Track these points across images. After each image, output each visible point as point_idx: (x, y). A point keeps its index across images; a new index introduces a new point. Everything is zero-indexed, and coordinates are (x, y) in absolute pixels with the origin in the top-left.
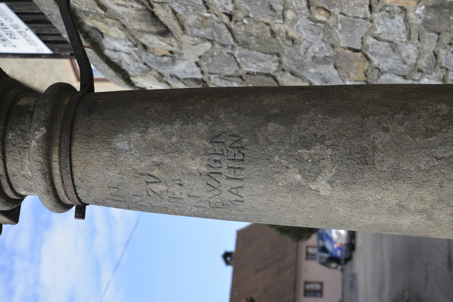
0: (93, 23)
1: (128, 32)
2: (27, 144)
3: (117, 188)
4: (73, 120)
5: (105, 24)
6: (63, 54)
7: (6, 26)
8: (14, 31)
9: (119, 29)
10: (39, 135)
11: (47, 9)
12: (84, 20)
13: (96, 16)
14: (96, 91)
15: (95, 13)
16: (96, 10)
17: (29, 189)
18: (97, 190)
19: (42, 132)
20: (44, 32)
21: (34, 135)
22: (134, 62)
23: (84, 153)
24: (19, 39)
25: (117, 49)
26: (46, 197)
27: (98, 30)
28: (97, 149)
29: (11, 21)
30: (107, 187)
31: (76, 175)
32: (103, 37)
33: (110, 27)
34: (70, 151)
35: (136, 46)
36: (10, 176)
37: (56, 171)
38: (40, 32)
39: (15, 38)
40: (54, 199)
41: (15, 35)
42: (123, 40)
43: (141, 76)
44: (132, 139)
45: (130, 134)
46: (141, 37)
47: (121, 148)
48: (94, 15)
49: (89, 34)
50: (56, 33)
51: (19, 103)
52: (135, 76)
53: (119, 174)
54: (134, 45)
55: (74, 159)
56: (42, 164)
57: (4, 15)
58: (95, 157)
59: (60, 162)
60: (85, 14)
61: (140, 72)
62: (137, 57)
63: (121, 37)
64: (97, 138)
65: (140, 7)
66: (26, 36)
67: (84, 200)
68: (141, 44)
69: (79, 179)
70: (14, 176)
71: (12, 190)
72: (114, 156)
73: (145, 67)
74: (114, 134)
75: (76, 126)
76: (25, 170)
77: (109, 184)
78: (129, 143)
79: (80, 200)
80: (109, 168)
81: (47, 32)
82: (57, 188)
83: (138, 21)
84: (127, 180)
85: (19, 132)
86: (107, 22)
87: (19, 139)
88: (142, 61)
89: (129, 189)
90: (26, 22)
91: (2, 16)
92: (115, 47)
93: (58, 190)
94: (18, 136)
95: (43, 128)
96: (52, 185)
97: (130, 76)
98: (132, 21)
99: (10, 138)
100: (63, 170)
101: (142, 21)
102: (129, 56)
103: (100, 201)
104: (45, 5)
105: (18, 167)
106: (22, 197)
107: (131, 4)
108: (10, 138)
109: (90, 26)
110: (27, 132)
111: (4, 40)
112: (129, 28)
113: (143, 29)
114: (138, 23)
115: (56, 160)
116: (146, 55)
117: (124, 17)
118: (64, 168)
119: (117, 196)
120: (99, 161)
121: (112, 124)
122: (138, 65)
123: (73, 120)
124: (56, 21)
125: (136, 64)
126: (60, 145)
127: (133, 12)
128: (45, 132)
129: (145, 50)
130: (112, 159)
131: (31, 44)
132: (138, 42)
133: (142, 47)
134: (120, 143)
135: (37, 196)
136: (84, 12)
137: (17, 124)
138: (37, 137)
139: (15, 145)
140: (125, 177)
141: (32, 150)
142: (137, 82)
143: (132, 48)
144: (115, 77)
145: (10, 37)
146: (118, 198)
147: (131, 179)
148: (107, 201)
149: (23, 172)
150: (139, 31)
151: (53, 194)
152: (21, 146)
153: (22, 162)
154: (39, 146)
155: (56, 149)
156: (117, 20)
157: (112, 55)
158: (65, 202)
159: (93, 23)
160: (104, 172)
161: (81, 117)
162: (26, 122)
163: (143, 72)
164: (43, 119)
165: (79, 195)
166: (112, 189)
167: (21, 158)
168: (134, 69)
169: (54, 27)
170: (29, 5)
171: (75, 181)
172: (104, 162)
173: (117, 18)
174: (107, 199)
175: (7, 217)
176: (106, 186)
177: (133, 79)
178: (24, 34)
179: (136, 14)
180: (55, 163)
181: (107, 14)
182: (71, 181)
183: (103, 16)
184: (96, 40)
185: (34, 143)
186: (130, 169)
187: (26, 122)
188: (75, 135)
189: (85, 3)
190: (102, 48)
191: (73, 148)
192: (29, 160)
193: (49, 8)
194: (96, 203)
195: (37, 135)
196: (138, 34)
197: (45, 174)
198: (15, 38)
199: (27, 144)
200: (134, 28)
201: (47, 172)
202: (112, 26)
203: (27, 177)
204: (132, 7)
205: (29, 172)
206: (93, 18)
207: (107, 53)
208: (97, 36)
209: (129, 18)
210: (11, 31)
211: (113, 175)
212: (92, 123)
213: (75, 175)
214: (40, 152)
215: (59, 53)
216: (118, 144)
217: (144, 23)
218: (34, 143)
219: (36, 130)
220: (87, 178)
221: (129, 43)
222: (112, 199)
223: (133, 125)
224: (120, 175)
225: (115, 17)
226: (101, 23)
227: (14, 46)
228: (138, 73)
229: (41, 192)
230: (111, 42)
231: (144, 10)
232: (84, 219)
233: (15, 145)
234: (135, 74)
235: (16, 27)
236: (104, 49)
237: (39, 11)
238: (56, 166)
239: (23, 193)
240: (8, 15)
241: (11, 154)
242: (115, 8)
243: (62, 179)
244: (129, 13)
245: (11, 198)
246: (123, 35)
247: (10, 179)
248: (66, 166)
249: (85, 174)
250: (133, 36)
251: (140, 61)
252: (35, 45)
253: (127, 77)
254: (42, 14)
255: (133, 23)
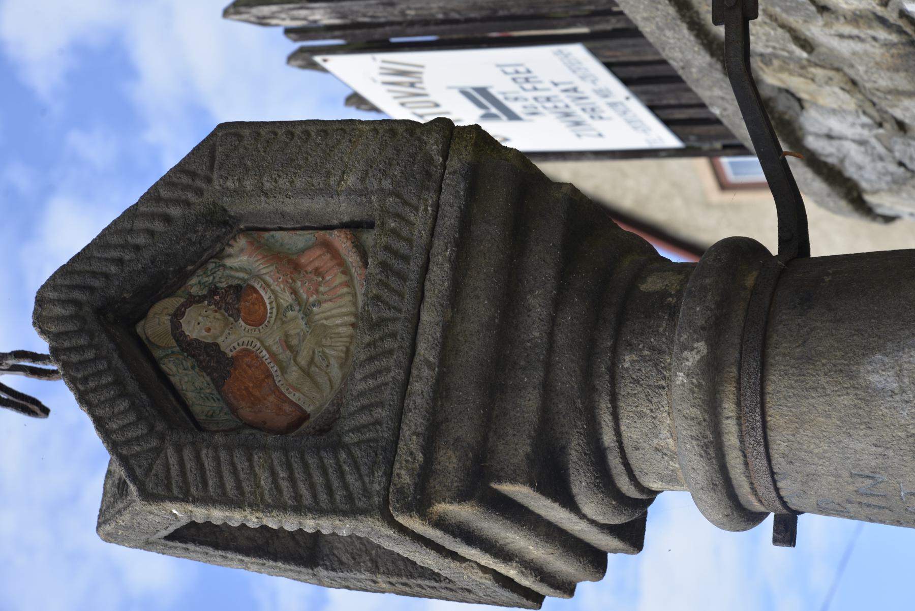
0: (781, 80)
1: (864, 95)
2: (664, 378)
3: (873, 478)
4: (767, 322)
5: (809, 81)
6: (706, 146)
7: (582, 92)
8: (601, 103)
9: (843, 89)
10: (692, 359)
11: (678, 55)
12: (761, 73)
13: (788, 64)
14: (813, 254)
15: (786, 57)
16: (788, 52)
17: (669, 479)
18: (824, 483)
19: (699, 352)
20: (665, 102)
21: (680, 359)
22: (873, 161)
23: (794, 399)
24: (610, 119)
25: (833, 134)
26: (709, 498)
27: (793, 95)
28: (824, 388)
29: (594, 82)
30: (848, 475)
31: (775, 447)
32: (802, 108)
33: (820, 86)
34: (763, 394)
35: (880, 125)
36: (628, 450)
37: (731, 439)
38: (657, 103)
39: (601, 118)
40: (725, 501)
41: (603, 112)
42: (850, 112)
43: (890, 190)
44: (906, 366)
45: (901, 354)
46: (893, 106)
47: (880, 386)
48: (784, 62)
49: (771, 104)
50: (694, 102)
51: (643, 287)
52: (875, 192)
53: (875, 445)
54: (876, 123)
55: (770, 412)
56: (699, 424)
57: (579, 69)
58: (820, 408)
59: (739, 418)
60: (762, 61)
61: (888, 183)
62: (881, 149)
63: (845, 107)
64: (824, 365)
65: (894, 38)
66: (625, 113)
67: (794, 503)
68: (893, 122)
69: (784, 456)
70: (637, 449)
71: (631, 480)
72: (863, 405)
73: (902, 170)
74: (863, 355)
75: (775, 337)
76: (662, 436)
77: (854, 467)
78: (899, 375)
79: (784, 504)
80: (852, 432)
81: (673, 102)
82: (732, 476)
83: (888, 69)
84: (896, 460)
85: (646, 352)
86: (814, 75)
87: (647, 369)
88: (894, 158)
89: (901, 480)
90: (627, 82)
91: (574, 72)
92: (830, 129)
93: (734, 482)
94: (645, 361)
95: (700, 344)
96: (723, 470)
97: (865, 191)
98: (874, 70)
99: (627, 365)
100: (747, 438)
101: (897, 70)
102: (862, 149)
103: (831, 506)
104: (673, 48)
105: (646, 430)
106: (652, 494)
107: (871, 32)
108: (627, 365)
109: (773, 87)
110: (664, 352)
111: (577, 124)
112: (864, 87)
113: (900, 88)
114: (888, 74)
115: (731, 414)
116: (903, 144)
117: (854, 62)
118: (748, 433)
119: (872, 495)
120: (829, 416)
121: (858, 330)
122: (884, 167)
123: (767, 322)
124: (698, 80)
125: (880, 165)
126: (739, 382)
127: (877, 51)
128: (705, 351)
129: (902, 133)
130: (860, 412)
131: (636, 128)
132: (885, 116)
133: (896, 127)
134: (879, 375)
135: (688, 494)
136: (762, 55)
137: (642, 334)
138: (687, 363)
139: (638, 382)
140: (890, 453)
141: (677, 393)
142: (879, 205)
143: (870, 130)
144: (829, 195)
145: (592, 117)
146: (874, 501)
147: (905, 458)
148: (849, 506)
149: (656, 441)
150: (890, 92)
151: (724, 491)
152: (651, 382)
153: (654, 418)
154: (692, 383)
155: (730, 389)
156: (838, 70)
157: (823, 148)
158: (750, 508)
159: (781, 80)
160: (840, 442)
161: (784, 317)
162: (661, 330)
163: (895, 182)
164: (700, 322)
165: (782, 493)
166: (861, 480)
167: (652, 411)
168: (873, 177)
169: (689, 90)
170: (634, 46)
171: (773, 462)
172: (840, 419)
173: (836, 65)
174: (849, 501)
175: (619, 537)
176: (845, 474)
177: (870, 199)
178: (620, 108)
179: (883, 54)
180: (729, 421)
181: (813, 58)
182: (765, 462)
183: (805, 62)
184: (787, 117)
185: (681, 378)
186: (903, 435)
187: (661, 330)
188: (773, 358)
189: (764, 38)
190: (800, 133)
191: (770, 388)
192: (669, 413)
193: (682, 53)
194: (821, 510)
195: (688, 360)
196: (886, 99)
197: (706, 445)
198: (601, 118)
199: (664, 378)
200: (876, 86)
201: (711, 442)
202: (827, 83)
203: (665, 451)
204: (875, 39)
205: (670, 441)
206: (782, 69)
207: (812, 143)
208: (789, 108)
209: (867, 65)
210: (593, 103)
211: (862, 448)
212: (812, 330)
213: (773, 447)
214: (695, 398)
215: (697, 144)
216: (874, 378)
217: (903, 74)
218: (681, 378)
219: (684, 347)
220: (803, 455)
221: (865, 119)
222: (860, 503)
223: (907, 332)
224: (880, 449)
225: (831, 65)
226: (801, 80)
227: (600, 135)
228: (884, 186)
229: (697, 486)
230: (820, 118)
231: (903, 44)
232: (794, 546)
233: (638, 382)
234: (877, 186)
235: (605, 94)
236: (804, 135)
237: (656, 58)
238: (730, 427)
239: (655, 486)
240: (586, 69)
241: (630, 401)
242: (835, 43)
243: (745, 456)
244: (866, 53)
245: (629, 498)
246: (849, 102)
247: (628, 456)
248: (753, 428)
249: (796, 446)
250: (874, 104)
251: (891, 159)
252: (646, 130)
253: (855, 194)
254: (664, 62)
255: (876, 76)
